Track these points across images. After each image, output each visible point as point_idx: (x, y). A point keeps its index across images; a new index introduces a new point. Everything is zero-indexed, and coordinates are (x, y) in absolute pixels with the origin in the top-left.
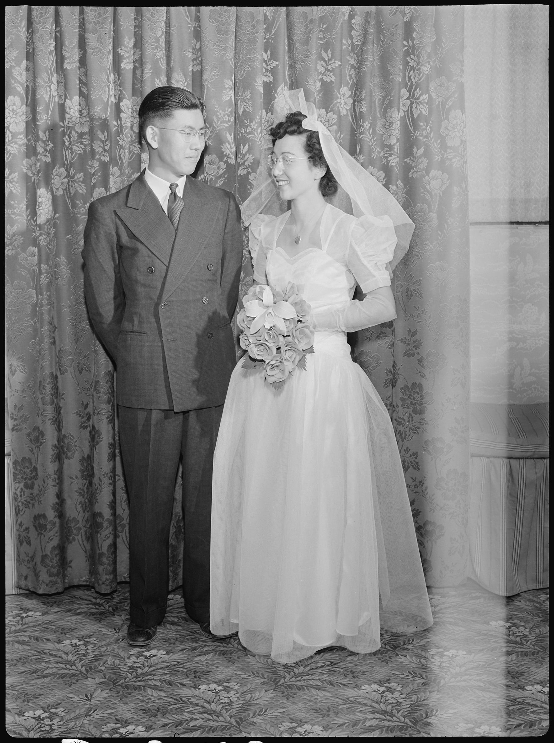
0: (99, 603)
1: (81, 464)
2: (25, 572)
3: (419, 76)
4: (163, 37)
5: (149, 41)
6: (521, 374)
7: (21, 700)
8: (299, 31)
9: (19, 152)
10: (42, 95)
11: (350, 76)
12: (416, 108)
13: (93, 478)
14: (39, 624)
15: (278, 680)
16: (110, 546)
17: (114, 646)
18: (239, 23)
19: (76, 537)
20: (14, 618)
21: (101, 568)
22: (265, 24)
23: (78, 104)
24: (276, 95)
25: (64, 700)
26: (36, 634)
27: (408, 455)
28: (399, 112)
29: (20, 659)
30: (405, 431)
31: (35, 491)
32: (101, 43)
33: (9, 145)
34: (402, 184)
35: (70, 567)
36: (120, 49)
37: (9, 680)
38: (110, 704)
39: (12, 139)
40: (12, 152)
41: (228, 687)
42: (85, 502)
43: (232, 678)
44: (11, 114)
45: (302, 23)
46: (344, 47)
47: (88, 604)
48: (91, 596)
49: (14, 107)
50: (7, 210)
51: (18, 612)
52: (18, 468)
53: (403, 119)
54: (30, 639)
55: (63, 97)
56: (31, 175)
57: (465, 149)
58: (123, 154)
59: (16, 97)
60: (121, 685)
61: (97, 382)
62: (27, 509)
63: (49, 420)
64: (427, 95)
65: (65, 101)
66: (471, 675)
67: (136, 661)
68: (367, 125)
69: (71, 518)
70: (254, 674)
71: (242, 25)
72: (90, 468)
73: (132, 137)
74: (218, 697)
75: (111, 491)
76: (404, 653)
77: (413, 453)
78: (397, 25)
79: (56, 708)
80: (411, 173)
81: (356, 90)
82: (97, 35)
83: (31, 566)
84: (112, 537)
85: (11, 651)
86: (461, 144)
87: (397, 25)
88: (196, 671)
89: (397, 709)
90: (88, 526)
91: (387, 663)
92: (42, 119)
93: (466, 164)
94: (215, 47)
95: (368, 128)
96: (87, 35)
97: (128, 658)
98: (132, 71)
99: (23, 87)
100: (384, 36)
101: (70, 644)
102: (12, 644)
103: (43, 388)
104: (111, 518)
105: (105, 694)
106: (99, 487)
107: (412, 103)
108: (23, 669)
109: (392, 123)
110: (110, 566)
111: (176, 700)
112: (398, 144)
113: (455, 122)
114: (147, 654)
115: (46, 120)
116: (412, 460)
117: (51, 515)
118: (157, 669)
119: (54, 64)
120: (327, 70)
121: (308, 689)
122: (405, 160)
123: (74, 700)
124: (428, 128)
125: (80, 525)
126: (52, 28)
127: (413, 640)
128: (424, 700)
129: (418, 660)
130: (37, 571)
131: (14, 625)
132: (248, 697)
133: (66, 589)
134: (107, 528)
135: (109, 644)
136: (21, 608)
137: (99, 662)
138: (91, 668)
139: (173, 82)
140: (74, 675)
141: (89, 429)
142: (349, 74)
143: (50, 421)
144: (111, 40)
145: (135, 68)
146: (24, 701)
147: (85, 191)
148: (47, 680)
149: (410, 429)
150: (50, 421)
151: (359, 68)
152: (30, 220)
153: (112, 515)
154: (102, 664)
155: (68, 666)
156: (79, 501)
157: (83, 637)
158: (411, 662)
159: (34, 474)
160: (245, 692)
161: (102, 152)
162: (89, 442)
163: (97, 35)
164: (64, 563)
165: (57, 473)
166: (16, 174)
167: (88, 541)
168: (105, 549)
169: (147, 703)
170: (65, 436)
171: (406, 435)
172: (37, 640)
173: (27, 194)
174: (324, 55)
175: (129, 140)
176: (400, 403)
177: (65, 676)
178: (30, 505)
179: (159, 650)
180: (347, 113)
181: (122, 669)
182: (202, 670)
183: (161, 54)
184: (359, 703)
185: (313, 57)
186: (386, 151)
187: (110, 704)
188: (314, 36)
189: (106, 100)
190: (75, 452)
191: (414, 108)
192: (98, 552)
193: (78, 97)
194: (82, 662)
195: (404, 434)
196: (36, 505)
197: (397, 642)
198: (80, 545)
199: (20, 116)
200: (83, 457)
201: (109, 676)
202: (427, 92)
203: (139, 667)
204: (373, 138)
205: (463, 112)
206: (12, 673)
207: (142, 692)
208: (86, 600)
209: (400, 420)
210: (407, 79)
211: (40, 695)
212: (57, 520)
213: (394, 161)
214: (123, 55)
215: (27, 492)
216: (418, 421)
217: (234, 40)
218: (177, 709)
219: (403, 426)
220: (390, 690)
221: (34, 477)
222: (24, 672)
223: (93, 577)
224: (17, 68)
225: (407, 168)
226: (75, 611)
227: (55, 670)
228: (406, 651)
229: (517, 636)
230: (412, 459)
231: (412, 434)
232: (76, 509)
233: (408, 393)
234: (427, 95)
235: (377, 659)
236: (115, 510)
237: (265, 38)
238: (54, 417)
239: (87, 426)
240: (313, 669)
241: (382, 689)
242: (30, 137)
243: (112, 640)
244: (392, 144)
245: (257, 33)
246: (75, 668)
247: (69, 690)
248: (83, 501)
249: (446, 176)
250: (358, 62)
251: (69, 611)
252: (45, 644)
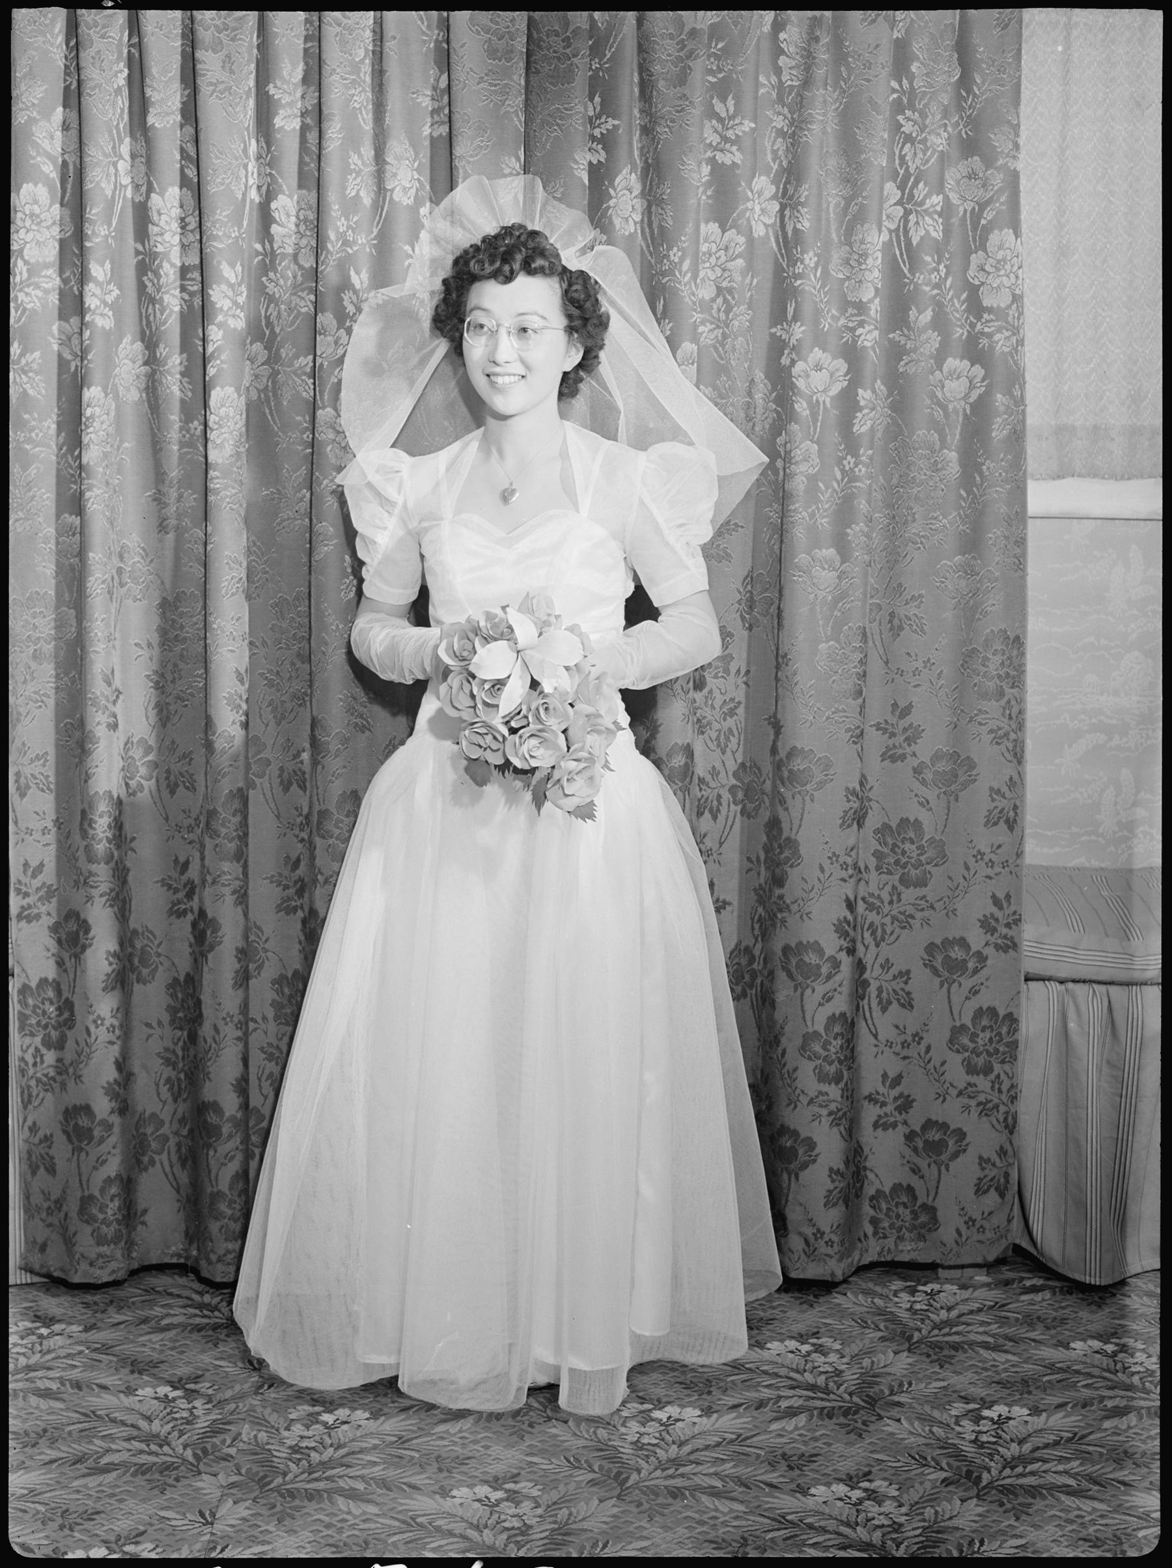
0: (209, 1305)
1: (171, 995)
2: (42, 1234)
3: (925, 154)
4: (367, 61)
5: (338, 70)
6: (1116, 804)
7: (54, 1526)
8: (665, 52)
9: (44, 306)
10: (98, 183)
11: (775, 152)
12: (917, 223)
13: (201, 1024)
15: (624, 1476)
16: (236, 1177)
17: (255, 1401)
18: (535, 35)
19: (157, 1158)
20: (22, 1338)
21: (214, 1227)
22: (590, 38)
23: (177, 203)
24: (611, 191)
25: (151, 1525)
26: (75, 1374)
27: (889, 976)
28: (880, 231)
29: (45, 1431)
30: (883, 924)
31: (69, 1055)
32: (232, 72)
33: (21, 290)
34: (882, 387)
35: (144, 1223)
36: (271, 85)
37: (16, 1481)
38: (256, 1532)
39: (29, 278)
40: (29, 306)
41: (515, 1492)
42: (179, 1080)
43: (523, 1472)
44: (28, 223)
45: (672, 38)
46: (762, 91)
47: (184, 1307)
48: (191, 1288)
49: (36, 207)
50: (15, 433)
51: (29, 1325)
52: (30, 1001)
53: (887, 247)
54: (63, 1384)
55: (144, 188)
56: (69, 357)
57: (1021, 314)
58: (275, 314)
59: (40, 185)
60: (277, 1490)
61: (212, 814)
62: (49, 1094)
63: (101, 896)
64: (941, 197)
65: (148, 197)
66: (1045, 1461)
67: (306, 1433)
68: (810, 259)
69: (147, 1115)
70: (569, 1461)
71: (541, 39)
72: (190, 1002)
73: (295, 277)
74: (495, 1516)
75: (240, 1056)
76: (895, 1412)
77: (900, 972)
78: (877, 46)
79: (137, 1543)
80: (902, 363)
81: (787, 182)
82: (221, 55)
83: (56, 1222)
84: (239, 1157)
85: (22, 1413)
86: (1013, 302)
87: (877, 46)
88: (439, 1457)
89: (893, 1540)
90: (185, 1132)
91: (860, 1435)
92: (97, 236)
93: (1023, 345)
94: (481, 85)
95: (812, 265)
96: (198, 54)
97: (288, 1429)
98: (298, 134)
99: (54, 166)
100: (850, 70)
101: (154, 1395)
103: (90, 826)
104: (239, 1115)
105: (243, 1511)
106: (214, 1045)
107: (907, 213)
108: (54, 1454)
109: (864, 255)
110: (235, 1221)
111: (404, 1522)
112: (877, 301)
113: (1000, 255)
114: (328, 1418)
115: (106, 237)
116: (897, 988)
117: (102, 1106)
118: (353, 1453)
119: (126, 117)
120: (725, 139)
121: (693, 1497)
122: (891, 336)
123: (174, 1523)
124: (941, 267)
125: (165, 1130)
126: (121, 38)
127: (910, 1384)
128: (951, 1518)
129: (927, 1428)
130: (70, 1233)
131: (24, 1354)
132: (563, 1514)
133: (133, 1273)
134: (230, 1137)
135: (241, 1397)
136: (35, 1316)
137: (222, 1437)
138: (205, 1451)
139: (388, 160)
140: (167, 1468)
141: (190, 917)
142: (772, 148)
143: (104, 899)
144: (253, 66)
145: (304, 129)
146: (62, 1527)
147: (190, 394)
148: (110, 1477)
149: (894, 919)
150: (104, 899)
151: (794, 137)
152: (65, 455)
153: (240, 1108)
154: (228, 1442)
155: (154, 1447)
156: (165, 1076)
157: (180, 1380)
158: (911, 1433)
159: (66, 1015)
160: (555, 1503)
161: (230, 308)
162: (191, 946)
163: (221, 55)
164: (130, 1214)
165: (119, 1015)
166: (37, 354)
167: (183, 1165)
168: (224, 1184)
169: (340, 1531)
170: (135, 932)
171: (884, 931)
172: (79, 1388)
173: (59, 398)
174: (719, 107)
175: (289, 283)
176: (872, 863)
177: (149, 1469)
178: (54, 1085)
179: (353, 1409)
180: (767, 233)
181: (275, 1453)
182: (454, 1455)
183: (363, 98)
184: (810, 1526)
185: (697, 112)
186: (852, 315)
187: (256, 1532)
188: (698, 66)
189: (240, 197)
190: (157, 967)
191: (911, 224)
192: (209, 1191)
193: (177, 189)
194: (185, 1437)
195: (880, 930)
196: (71, 1084)
197: (877, 1388)
198: (166, 1175)
199: (48, 228)
200: (176, 980)
201: (249, 1470)
202: (940, 188)
203: (313, 1448)
204: (823, 286)
205: (1017, 234)
206: (28, 1463)
207: (326, 1504)
208: (179, 1296)
209: (871, 900)
210: (897, 162)
211: (98, 1513)
212: (115, 1119)
213: (869, 337)
214: (280, 99)
215: (50, 1057)
216: (912, 901)
217: (523, 72)
218: (407, 1543)
219: (878, 913)
220: (872, 1495)
221: (66, 1021)
222: (55, 1461)
223: (195, 1246)
224: (41, 123)
225: (895, 353)
226: (158, 1322)
227: (125, 1456)
228: (897, 1409)
229: (1133, 1374)
230: (898, 985)
231: (897, 931)
232: (158, 1094)
233: (890, 841)
234: (941, 197)
235: (837, 1427)
236: (248, 1097)
237: (591, 69)
238: (112, 891)
239: (185, 911)
240: (697, 1450)
241: (856, 1494)
242: (68, 274)
243: (246, 1386)
244: (864, 300)
245: (575, 56)
246: (171, 1452)
247: (161, 1501)
248: (173, 1078)
249: (979, 371)
250: (791, 124)
251: (145, 1321)
252: (98, 1396)
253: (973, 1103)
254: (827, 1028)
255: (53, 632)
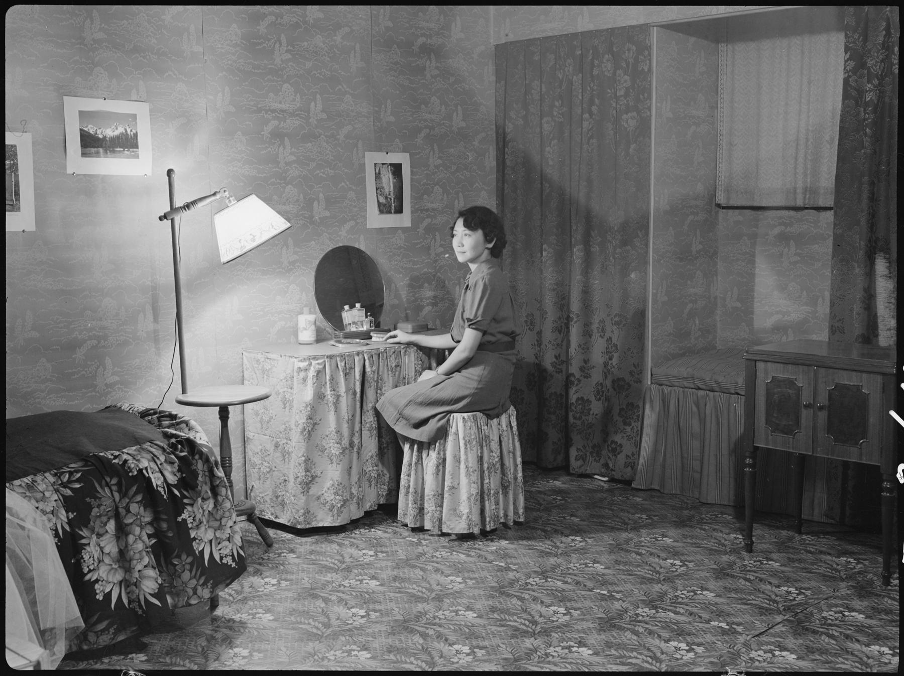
14: (705, 603)
54: (841, 634)
102: (820, 635)
181: (742, 657)
253: (625, 435)
254: (576, 401)
255: (159, 304)
